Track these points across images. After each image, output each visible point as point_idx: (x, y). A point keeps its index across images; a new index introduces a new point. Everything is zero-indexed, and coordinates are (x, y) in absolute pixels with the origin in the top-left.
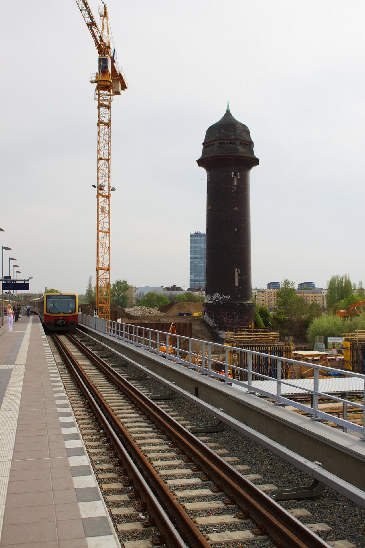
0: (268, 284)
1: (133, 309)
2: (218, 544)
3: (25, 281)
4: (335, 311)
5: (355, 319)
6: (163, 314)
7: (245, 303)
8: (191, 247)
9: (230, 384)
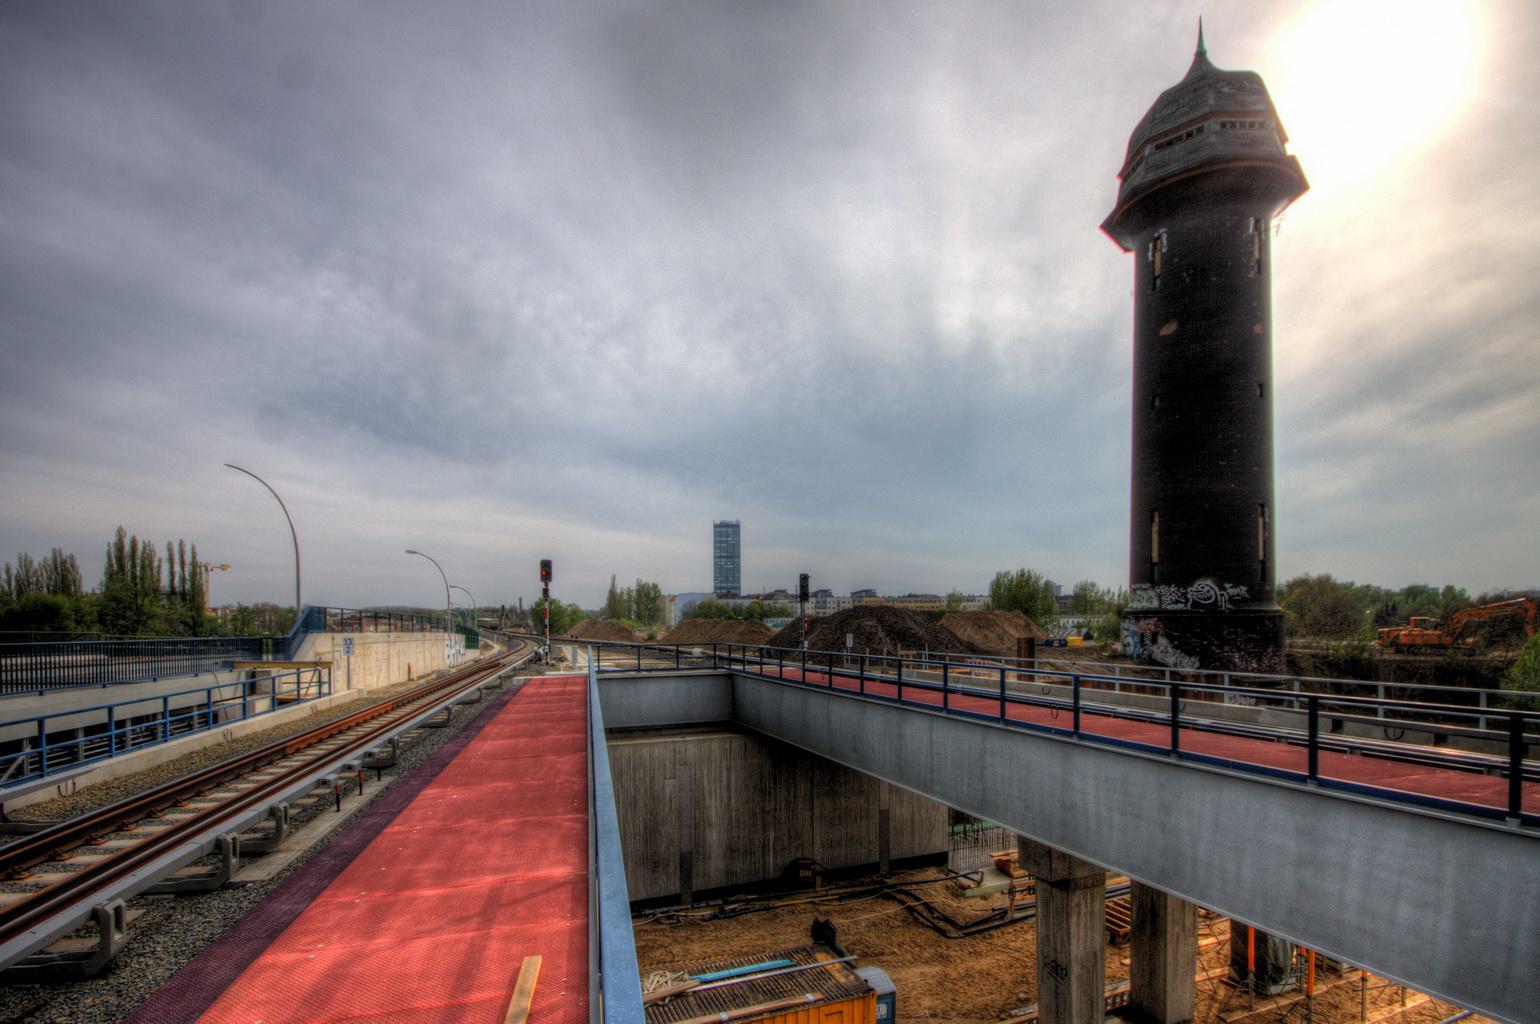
8: (715, 542)
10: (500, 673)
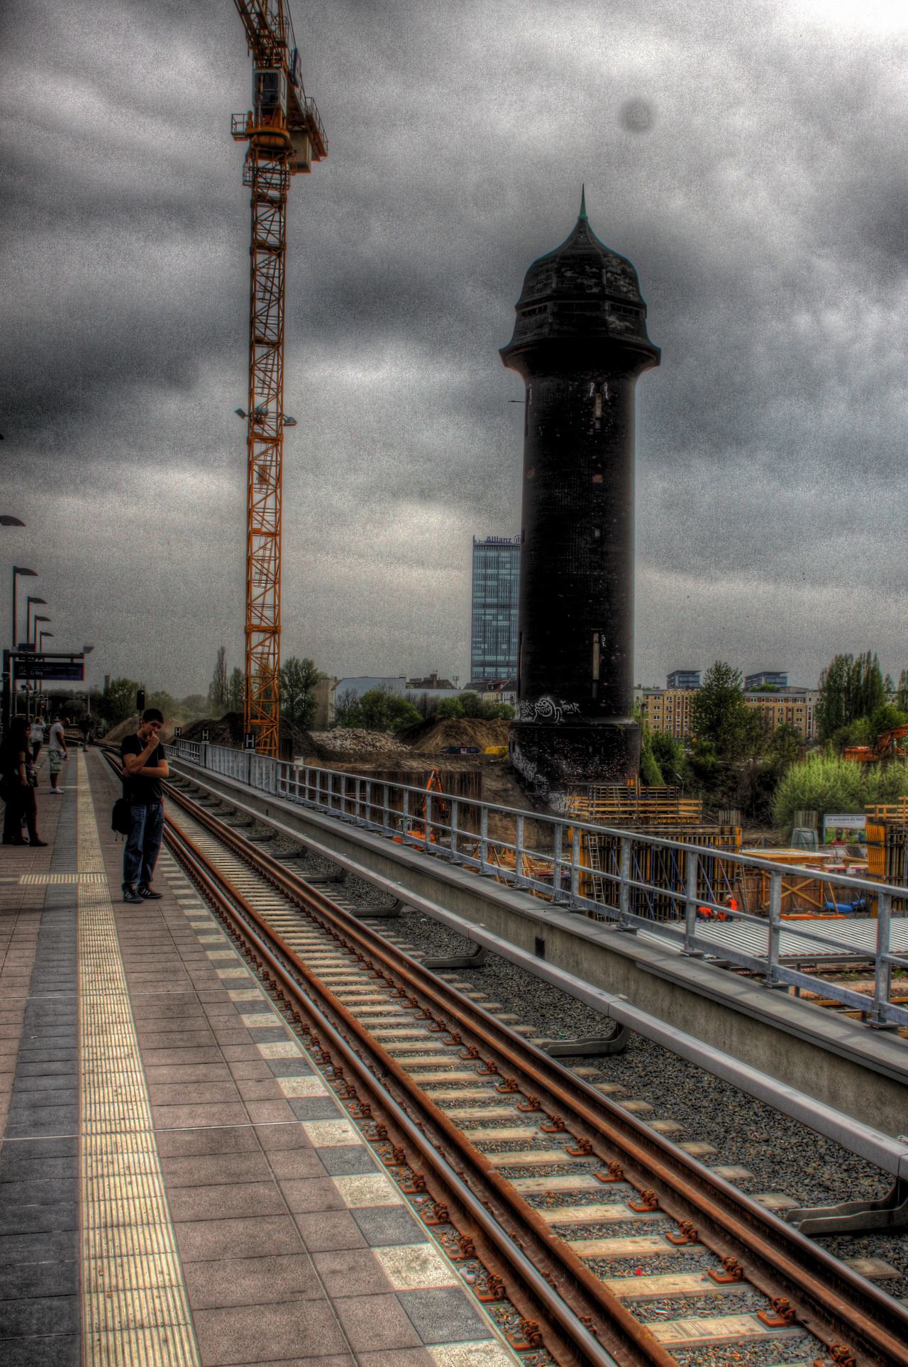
0: (669, 676)
1: (330, 735)
2: (677, 1350)
3: (72, 657)
4: (844, 746)
5: (894, 768)
6: (406, 749)
7: (616, 722)
8: (475, 577)
9: (633, 931)
10: (526, 955)
